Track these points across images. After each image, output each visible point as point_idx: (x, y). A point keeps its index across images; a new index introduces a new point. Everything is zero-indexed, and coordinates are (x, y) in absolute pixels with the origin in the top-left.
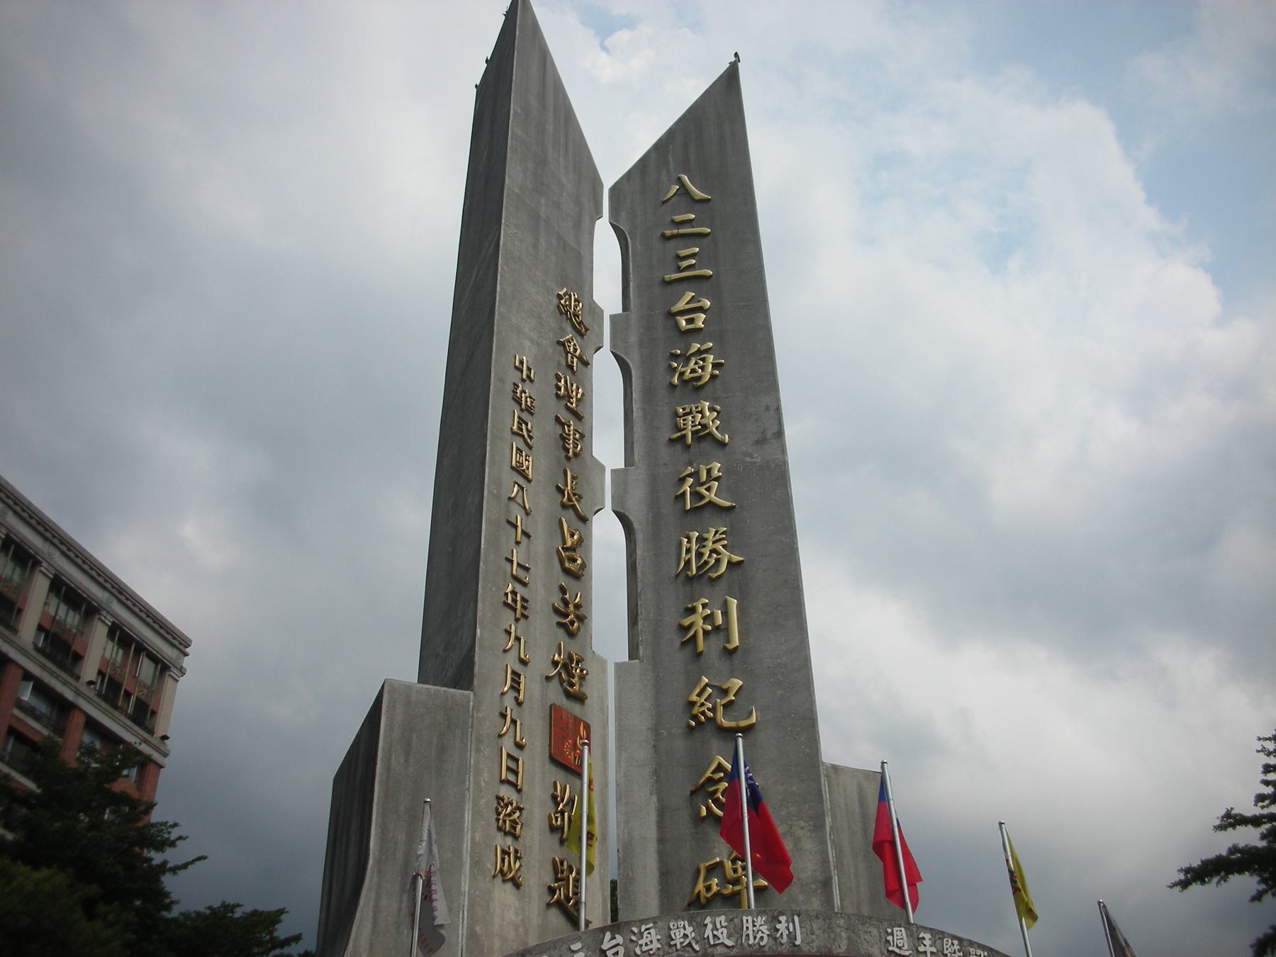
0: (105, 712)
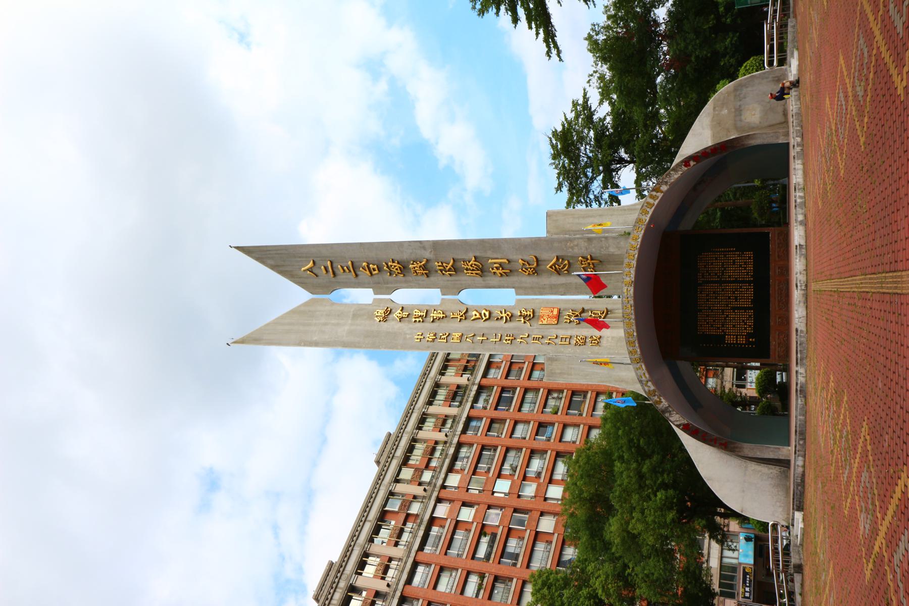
0: (478, 370)
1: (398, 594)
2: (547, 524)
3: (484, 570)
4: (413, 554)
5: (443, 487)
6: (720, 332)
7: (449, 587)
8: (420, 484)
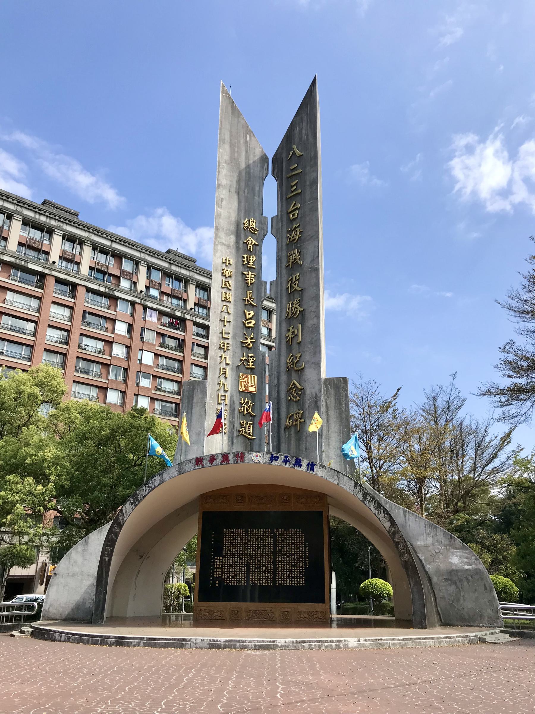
1: (47, 271)
2: (113, 397)
3: (71, 344)
4: (82, 283)
5: (145, 308)
6: (225, 551)
7: (55, 315)
8: (147, 287)
